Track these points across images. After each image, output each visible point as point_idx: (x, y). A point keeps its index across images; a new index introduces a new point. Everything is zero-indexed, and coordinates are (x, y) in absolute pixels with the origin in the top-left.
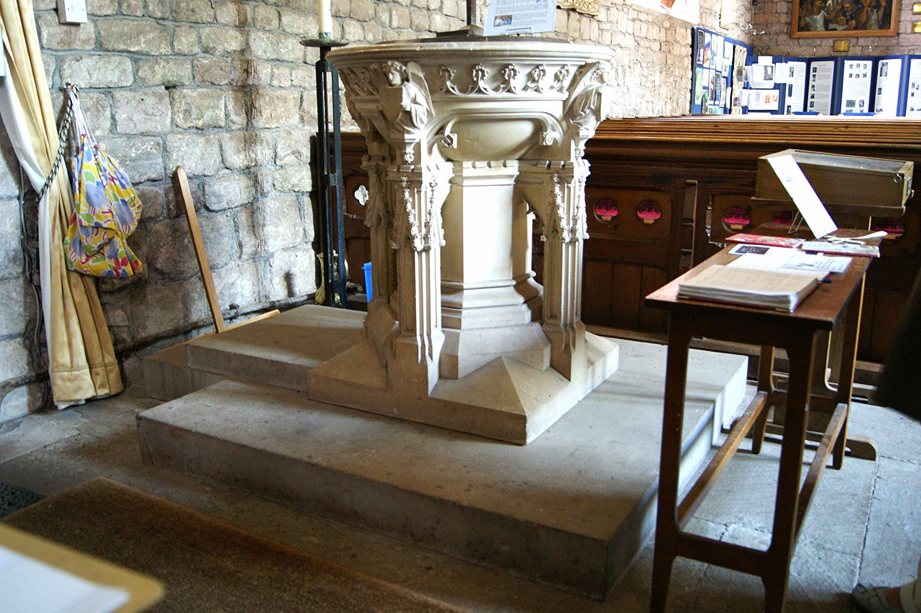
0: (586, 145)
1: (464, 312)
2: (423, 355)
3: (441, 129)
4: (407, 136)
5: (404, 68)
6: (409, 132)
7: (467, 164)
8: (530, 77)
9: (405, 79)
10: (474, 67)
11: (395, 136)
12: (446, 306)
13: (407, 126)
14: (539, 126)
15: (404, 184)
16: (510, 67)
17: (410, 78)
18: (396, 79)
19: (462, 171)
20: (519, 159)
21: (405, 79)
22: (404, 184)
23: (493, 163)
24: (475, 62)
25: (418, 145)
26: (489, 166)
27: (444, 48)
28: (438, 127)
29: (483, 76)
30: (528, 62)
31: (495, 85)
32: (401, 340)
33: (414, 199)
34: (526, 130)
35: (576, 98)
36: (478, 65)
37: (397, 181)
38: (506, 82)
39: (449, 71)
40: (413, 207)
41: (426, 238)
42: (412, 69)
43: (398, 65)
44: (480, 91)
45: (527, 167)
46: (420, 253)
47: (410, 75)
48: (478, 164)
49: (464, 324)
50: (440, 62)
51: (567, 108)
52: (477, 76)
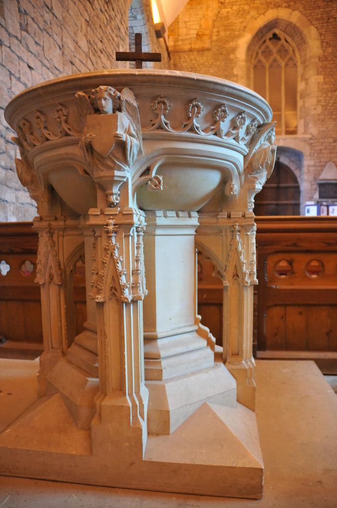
0: (255, 199)
1: (164, 363)
2: (135, 417)
3: (148, 171)
4: (117, 173)
5: (119, 94)
6: (120, 169)
7: (159, 213)
8: (233, 122)
9: (118, 108)
10: (191, 101)
11: (102, 174)
12: (147, 357)
13: (118, 159)
14: (226, 179)
15: (111, 228)
16: (223, 108)
17: (124, 108)
18: (108, 105)
19: (155, 220)
20: (198, 212)
21: (118, 108)
22: (111, 228)
23: (180, 214)
24: (194, 96)
25: (126, 184)
26: (178, 216)
27: (166, 74)
28: (144, 168)
29: (199, 113)
30: (236, 106)
31: (206, 125)
32: (107, 402)
33: (121, 244)
34: (213, 179)
35: (254, 154)
36: (195, 99)
37: (102, 226)
38: (215, 122)
39: (164, 103)
40: (121, 254)
41: (135, 287)
42: (127, 96)
43: (112, 90)
44: (192, 130)
45: (208, 219)
46: (127, 304)
47: (124, 104)
48: (169, 213)
49: (165, 375)
50: (157, 91)
51: (247, 163)
52: (193, 112)
